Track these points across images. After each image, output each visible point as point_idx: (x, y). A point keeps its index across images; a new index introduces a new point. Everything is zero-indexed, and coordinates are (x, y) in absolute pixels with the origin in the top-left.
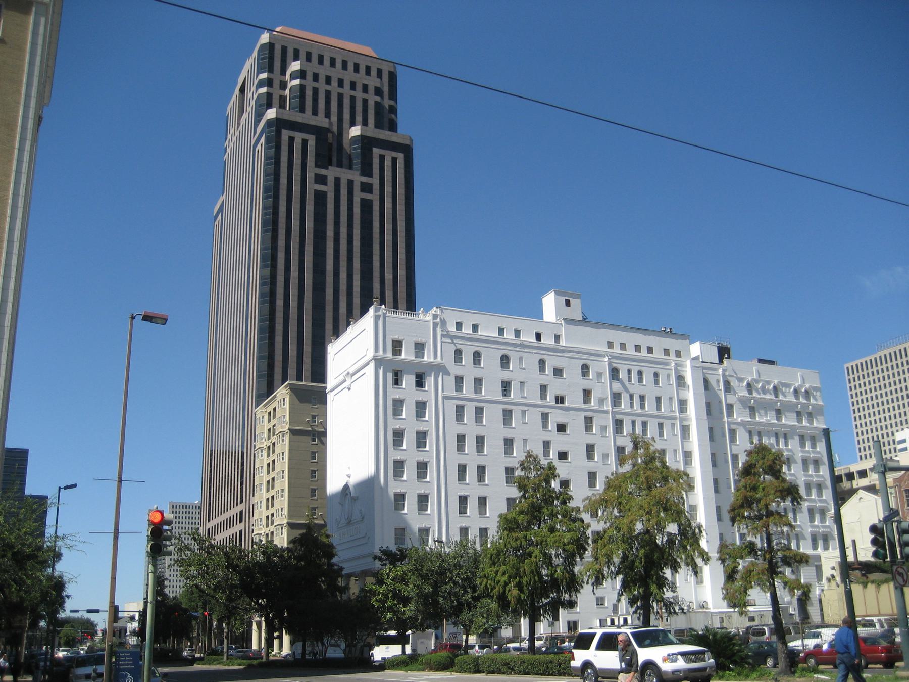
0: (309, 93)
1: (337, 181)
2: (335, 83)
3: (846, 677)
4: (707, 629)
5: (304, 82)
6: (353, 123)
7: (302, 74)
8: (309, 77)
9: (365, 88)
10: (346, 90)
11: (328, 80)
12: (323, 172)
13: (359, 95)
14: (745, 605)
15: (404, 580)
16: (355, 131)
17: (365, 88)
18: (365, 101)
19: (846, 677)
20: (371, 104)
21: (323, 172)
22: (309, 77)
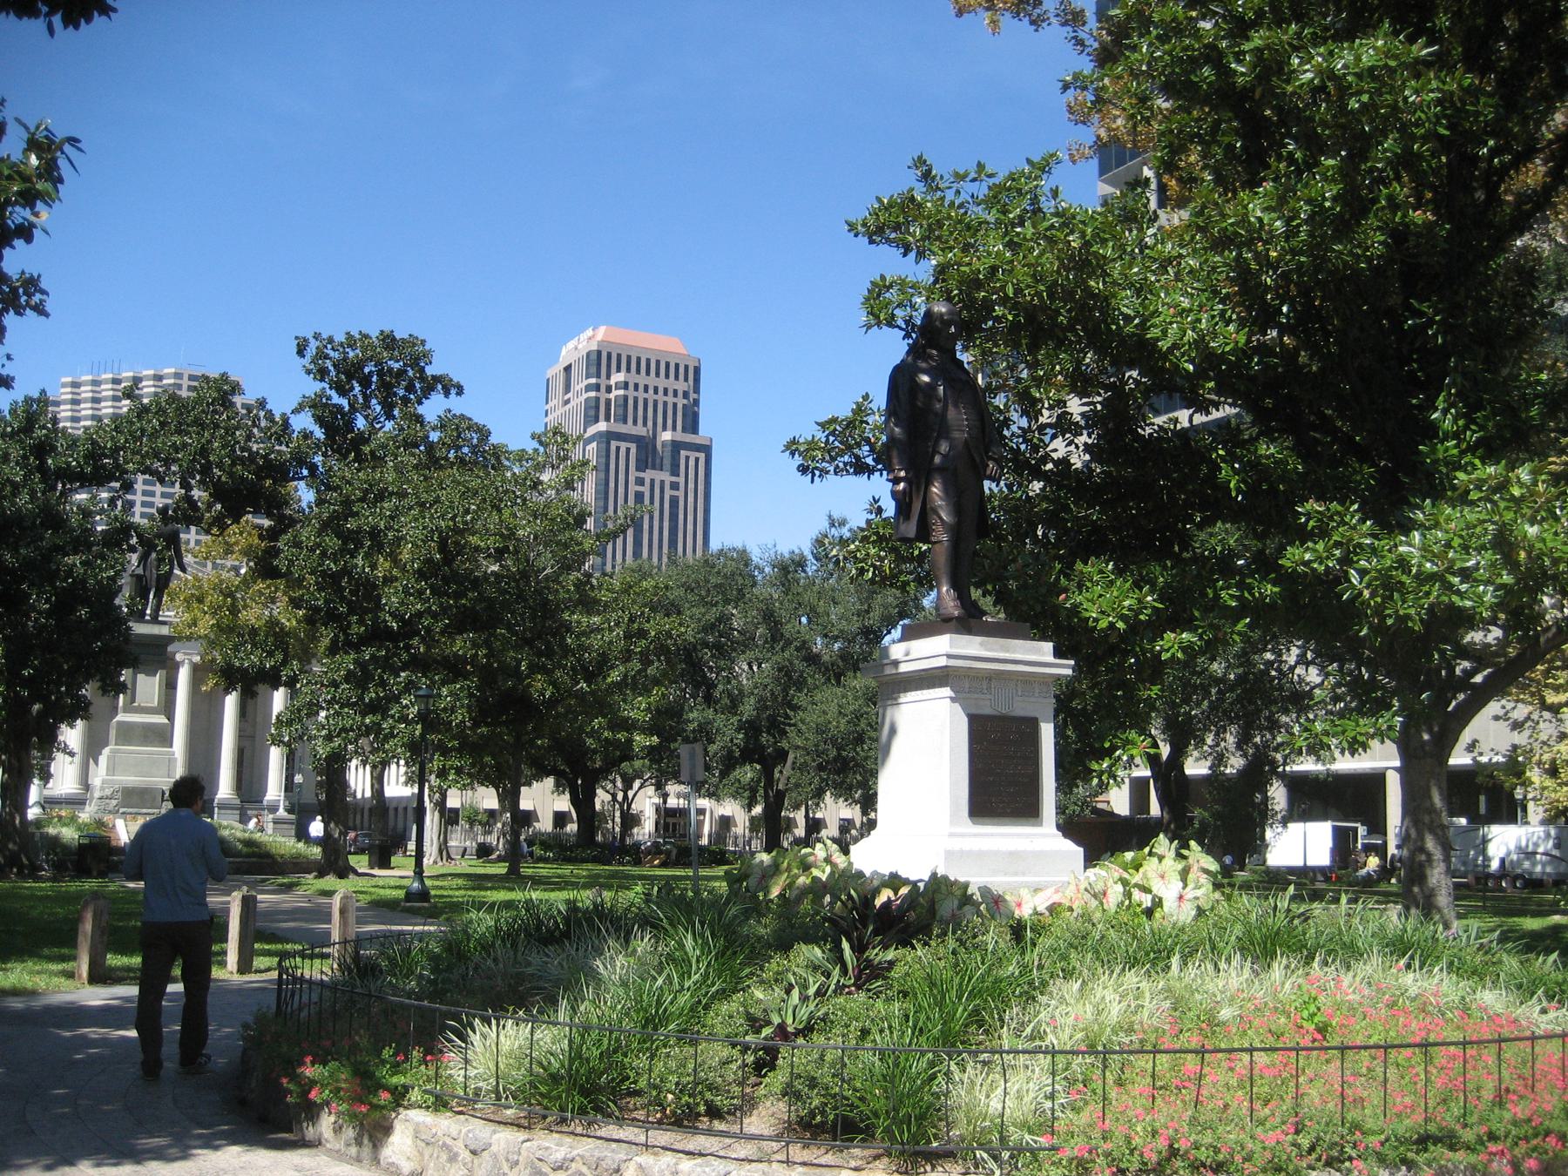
2: (651, 391)
6: (665, 429)
11: (646, 389)
12: (642, 475)
18: (675, 405)
20: (680, 407)
22: (631, 387)
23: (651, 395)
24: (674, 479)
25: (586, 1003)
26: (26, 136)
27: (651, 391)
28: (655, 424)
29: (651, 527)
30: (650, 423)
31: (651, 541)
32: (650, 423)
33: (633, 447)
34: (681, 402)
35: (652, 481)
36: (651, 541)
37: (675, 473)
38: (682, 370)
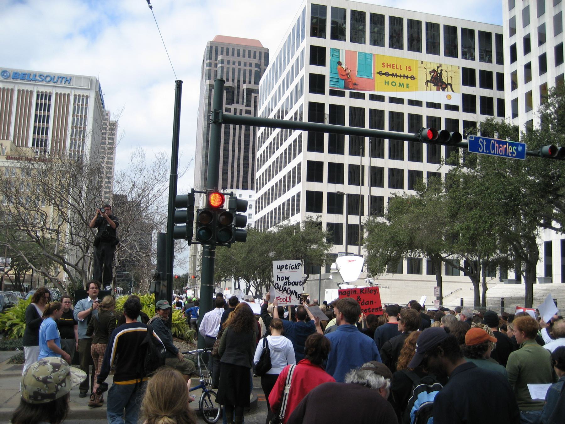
0: (225, 70)
1: (235, 110)
2: (237, 64)
3: (562, 196)
4: (338, 192)
5: (211, 61)
6: (244, 82)
7: (222, 62)
8: (225, 62)
9: (251, 65)
10: (242, 67)
11: (240, 64)
12: (229, 106)
13: (248, 68)
14: (79, 166)
15: (267, 241)
16: (245, 87)
17: (228, 62)
18: (250, 71)
19: (562, 196)
20: (253, 72)
21: (229, 106)
22: (225, 62)
23: (242, 67)
24: (248, 108)
25: (67, 241)
26: (459, 305)
27: (237, 64)
28: (239, 81)
29: (234, 134)
30: (236, 81)
31: (240, 144)
32: (236, 81)
33: (305, 134)
34: (254, 69)
35: (235, 110)
36: (234, 141)
37: (248, 105)
38: (258, 54)
